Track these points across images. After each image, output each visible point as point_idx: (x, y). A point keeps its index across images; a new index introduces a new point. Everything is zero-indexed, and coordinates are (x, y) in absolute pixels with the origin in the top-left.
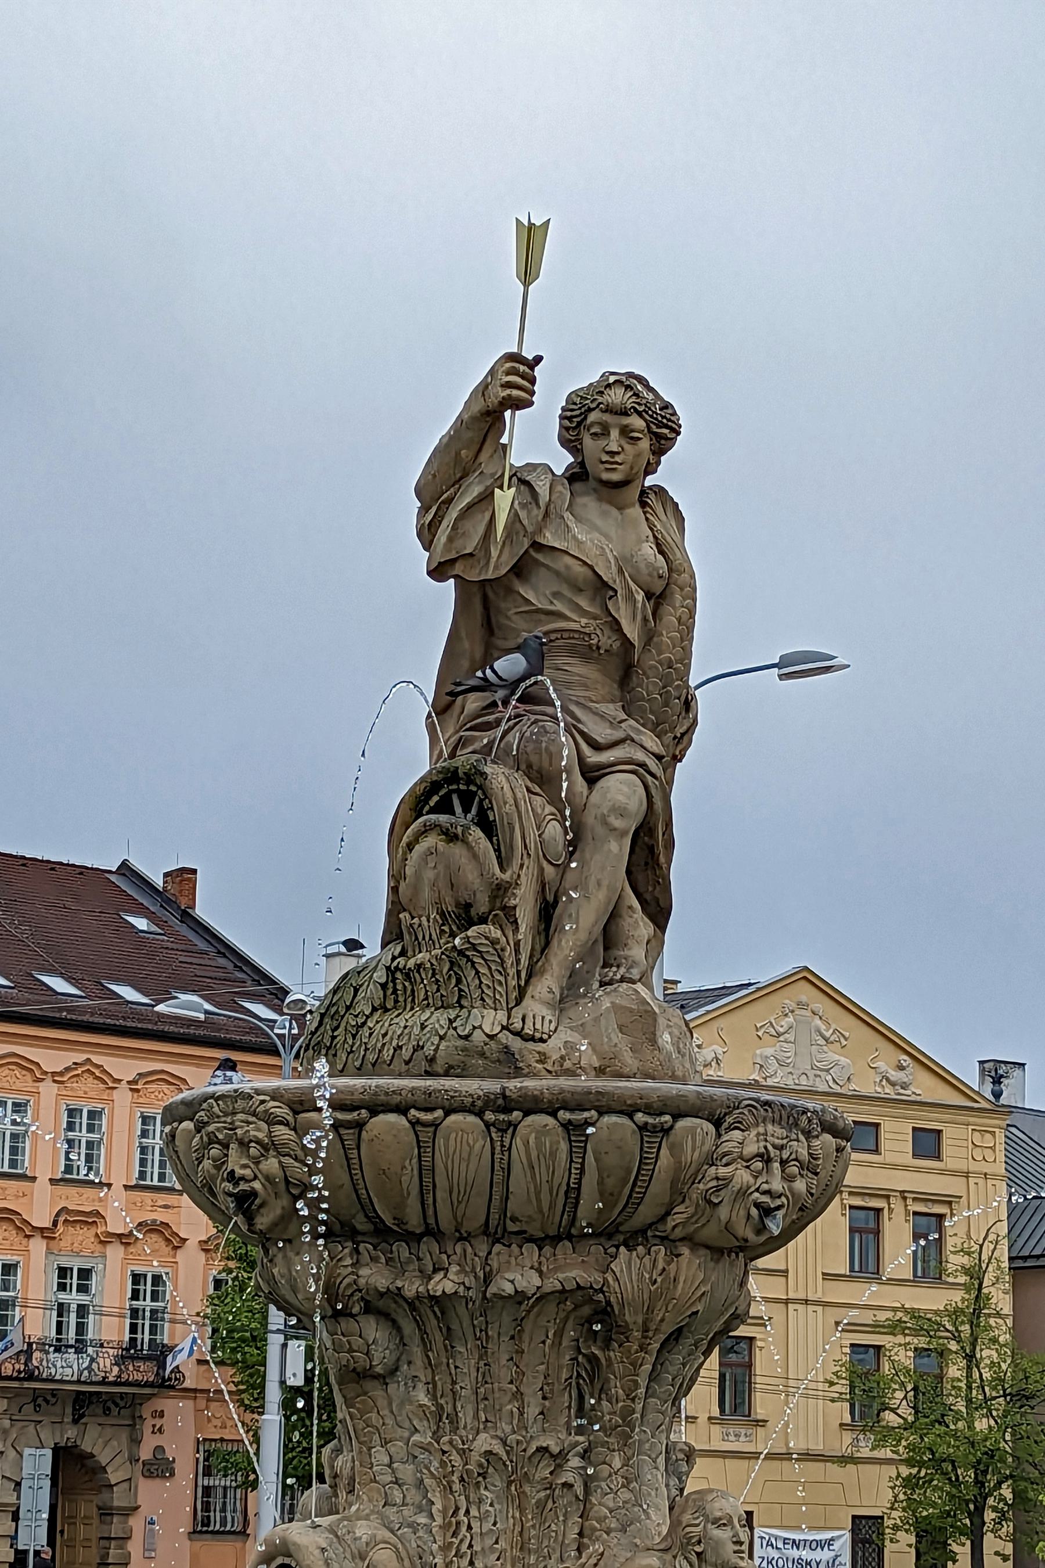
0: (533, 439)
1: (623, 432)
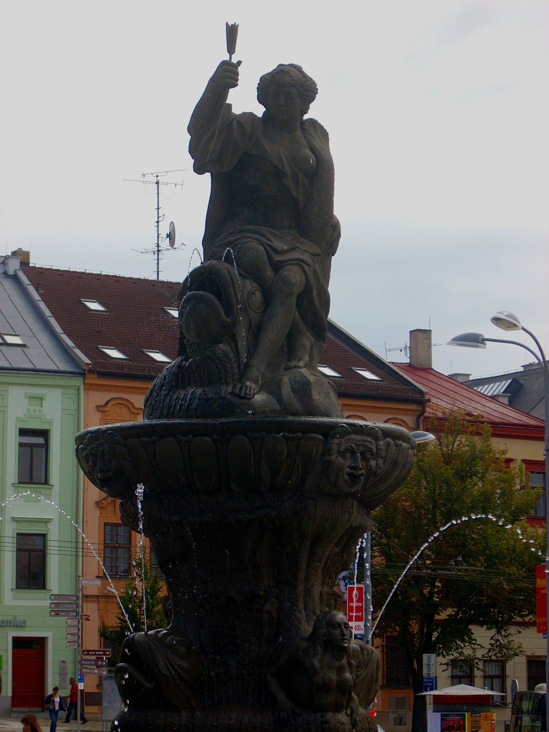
0: (244, 100)
1: (288, 90)
